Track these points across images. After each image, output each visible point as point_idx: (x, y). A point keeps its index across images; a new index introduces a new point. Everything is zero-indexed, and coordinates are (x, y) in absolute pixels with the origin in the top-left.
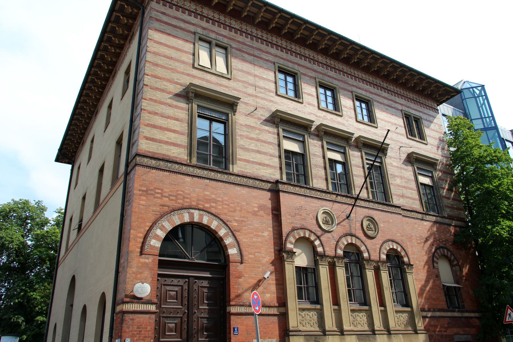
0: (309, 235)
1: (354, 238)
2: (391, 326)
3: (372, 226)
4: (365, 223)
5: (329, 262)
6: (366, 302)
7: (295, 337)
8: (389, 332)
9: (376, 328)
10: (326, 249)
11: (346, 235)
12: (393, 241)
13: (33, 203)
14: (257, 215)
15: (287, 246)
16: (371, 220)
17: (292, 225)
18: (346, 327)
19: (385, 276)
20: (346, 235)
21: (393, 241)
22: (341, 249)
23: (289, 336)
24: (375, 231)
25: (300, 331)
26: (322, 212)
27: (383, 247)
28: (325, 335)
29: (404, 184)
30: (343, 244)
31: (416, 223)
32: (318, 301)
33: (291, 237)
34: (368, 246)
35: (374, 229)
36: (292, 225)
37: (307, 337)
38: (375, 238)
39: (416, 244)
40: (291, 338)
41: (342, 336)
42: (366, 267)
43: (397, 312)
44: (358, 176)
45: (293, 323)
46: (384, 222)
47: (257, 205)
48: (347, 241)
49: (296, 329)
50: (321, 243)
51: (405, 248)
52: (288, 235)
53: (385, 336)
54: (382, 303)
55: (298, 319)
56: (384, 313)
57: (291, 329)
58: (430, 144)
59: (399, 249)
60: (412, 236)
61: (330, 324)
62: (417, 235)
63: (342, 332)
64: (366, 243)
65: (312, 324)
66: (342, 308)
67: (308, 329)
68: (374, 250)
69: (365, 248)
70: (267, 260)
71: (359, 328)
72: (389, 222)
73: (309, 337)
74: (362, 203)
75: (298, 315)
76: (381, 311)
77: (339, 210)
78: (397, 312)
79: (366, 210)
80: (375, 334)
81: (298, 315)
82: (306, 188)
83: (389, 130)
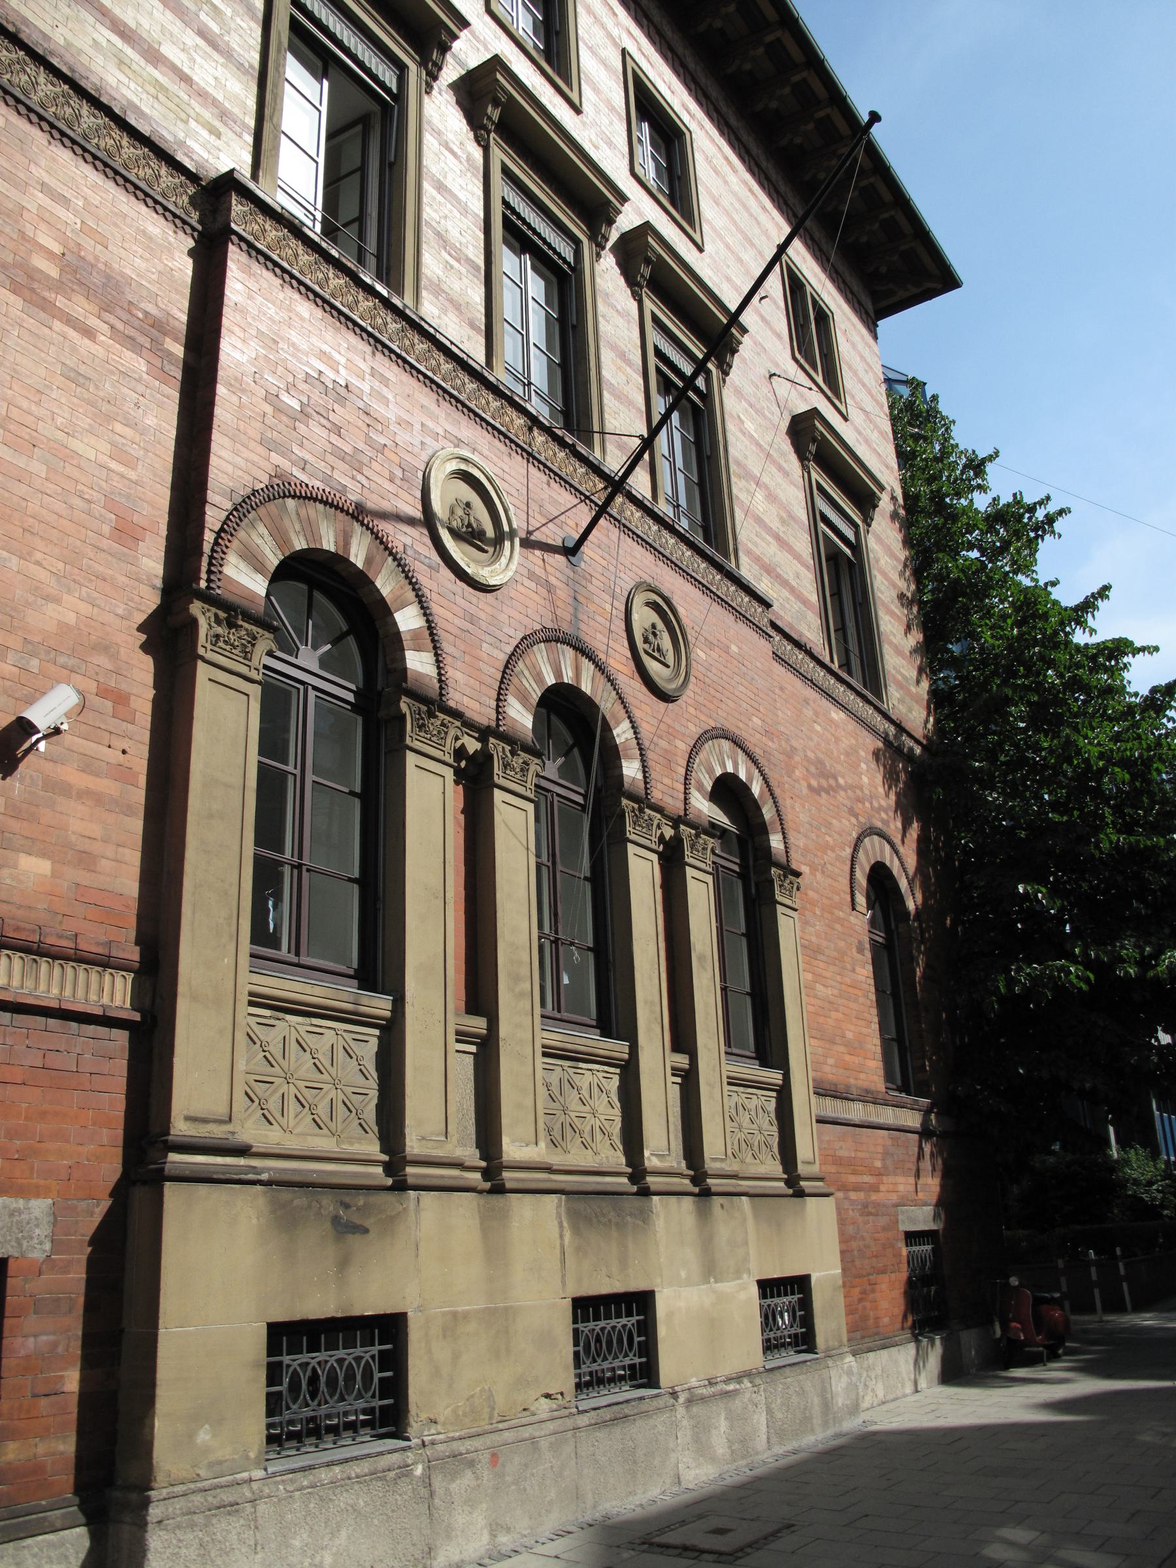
0: (369, 561)
1: (587, 667)
2: (708, 1153)
3: (666, 642)
4: (643, 617)
5: (460, 753)
6: (614, 1016)
7: (202, 1189)
8: (701, 1185)
9: (651, 1160)
10: (451, 673)
11: (554, 637)
12: (737, 743)
13: (144, 637)
14: (46, 306)
15: (228, 570)
16: (664, 609)
17: (276, 458)
18: (513, 1149)
19: (514, 824)
20: (554, 637)
21: (737, 743)
22: (523, 698)
23: (159, 1179)
24: (677, 674)
25: (243, 1151)
26: (454, 466)
27: (702, 756)
28: (401, 1186)
29: (775, 524)
30: (539, 678)
31: (806, 701)
32: (378, 962)
33: (262, 529)
34: (646, 730)
35: (671, 663)
36: (276, 458)
37: (286, 1194)
38: (673, 701)
39: (805, 791)
40: (170, 1191)
41: (497, 1200)
42: (631, 832)
43: (733, 1082)
44: (623, 401)
45: (199, 1089)
46: (710, 645)
47: (57, 249)
48: (558, 673)
49: (216, 1132)
50: (431, 627)
51: (777, 792)
52: (243, 508)
53: (688, 1202)
54: (682, 1036)
55: (241, 1065)
56: (689, 1081)
57: (180, 1128)
58: (852, 424)
59: (756, 789)
60: (794, 749)
61: (436, 1115)
62: (811, 755)
63: (495, 1177)
64: (637, 714)
65: (322, 1110)
66: (504, 1030)
67: (292, 1144)
68: (661, 755)
69: (630, 734)
70: (71, 618)
71: (578, 1157)
72: (727, 650)
73: (299, 1199)
74: (634, 515)
75: (241, 1037)
76: (676, 1071)
77: (533, 495)
78: (733, 1082)
79: (648, 558)
80: (645, 1192)
81: (241, 1037)
82: (387, 303)
83: (35, 1396)
